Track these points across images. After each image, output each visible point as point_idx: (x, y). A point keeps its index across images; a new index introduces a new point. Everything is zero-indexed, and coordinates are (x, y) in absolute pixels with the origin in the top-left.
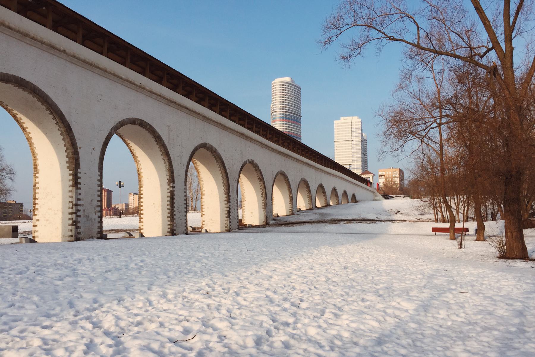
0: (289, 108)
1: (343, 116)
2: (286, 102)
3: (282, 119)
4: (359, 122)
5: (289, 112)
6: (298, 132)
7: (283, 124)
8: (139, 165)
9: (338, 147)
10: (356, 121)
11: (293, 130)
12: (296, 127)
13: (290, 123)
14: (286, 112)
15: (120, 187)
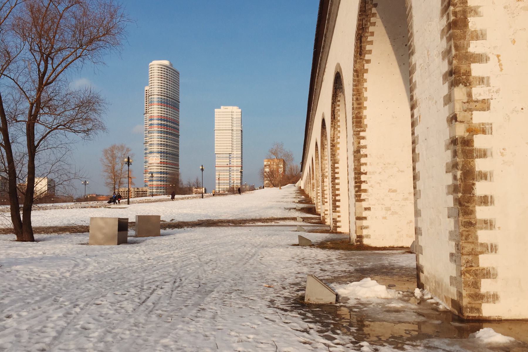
0: (167, 92)
1: (224, 106)
2: (164, 86)
3: (160, 103)
4: (239, 112)
5: (167, 97)
6: (176, 118)
7: (161, 108)
8: (336, 133)
9: (219, 136)
10: (236, 111)
11: (171, 116)
12: (174, 112)
13: (168, 108)
14: (164, 96)
15: (129, 166)
